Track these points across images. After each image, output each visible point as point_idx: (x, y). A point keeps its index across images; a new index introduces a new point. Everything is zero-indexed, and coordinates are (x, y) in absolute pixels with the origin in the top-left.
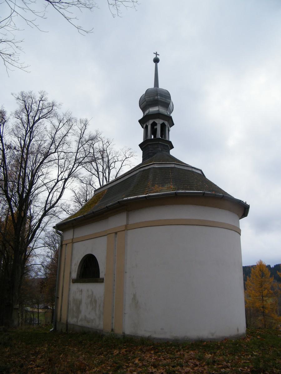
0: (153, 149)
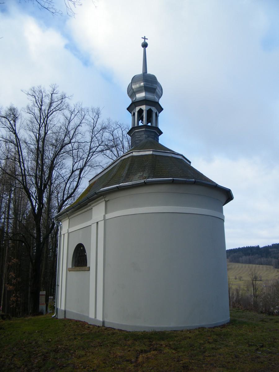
0: (140, 136)
